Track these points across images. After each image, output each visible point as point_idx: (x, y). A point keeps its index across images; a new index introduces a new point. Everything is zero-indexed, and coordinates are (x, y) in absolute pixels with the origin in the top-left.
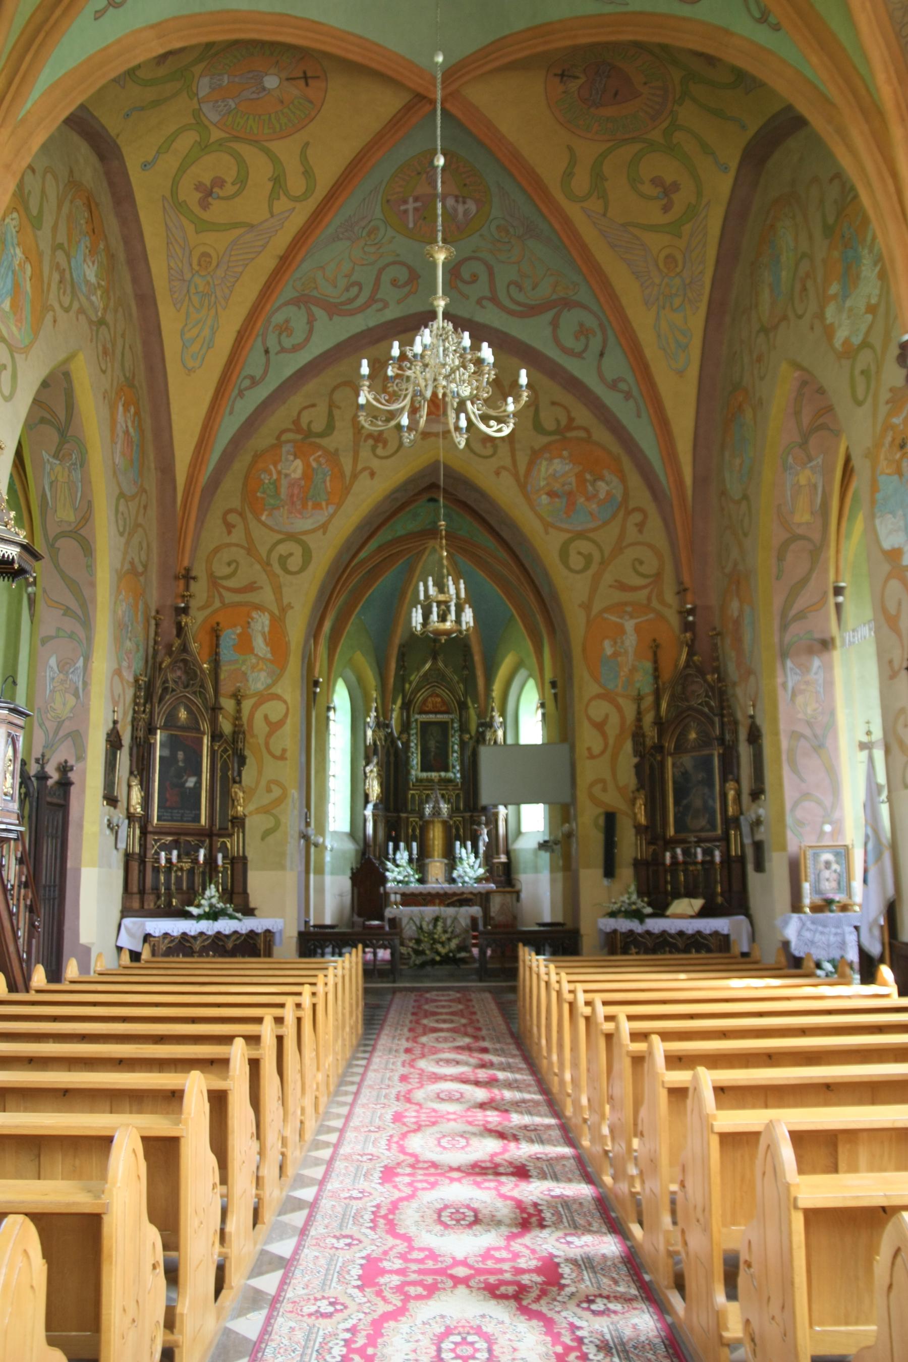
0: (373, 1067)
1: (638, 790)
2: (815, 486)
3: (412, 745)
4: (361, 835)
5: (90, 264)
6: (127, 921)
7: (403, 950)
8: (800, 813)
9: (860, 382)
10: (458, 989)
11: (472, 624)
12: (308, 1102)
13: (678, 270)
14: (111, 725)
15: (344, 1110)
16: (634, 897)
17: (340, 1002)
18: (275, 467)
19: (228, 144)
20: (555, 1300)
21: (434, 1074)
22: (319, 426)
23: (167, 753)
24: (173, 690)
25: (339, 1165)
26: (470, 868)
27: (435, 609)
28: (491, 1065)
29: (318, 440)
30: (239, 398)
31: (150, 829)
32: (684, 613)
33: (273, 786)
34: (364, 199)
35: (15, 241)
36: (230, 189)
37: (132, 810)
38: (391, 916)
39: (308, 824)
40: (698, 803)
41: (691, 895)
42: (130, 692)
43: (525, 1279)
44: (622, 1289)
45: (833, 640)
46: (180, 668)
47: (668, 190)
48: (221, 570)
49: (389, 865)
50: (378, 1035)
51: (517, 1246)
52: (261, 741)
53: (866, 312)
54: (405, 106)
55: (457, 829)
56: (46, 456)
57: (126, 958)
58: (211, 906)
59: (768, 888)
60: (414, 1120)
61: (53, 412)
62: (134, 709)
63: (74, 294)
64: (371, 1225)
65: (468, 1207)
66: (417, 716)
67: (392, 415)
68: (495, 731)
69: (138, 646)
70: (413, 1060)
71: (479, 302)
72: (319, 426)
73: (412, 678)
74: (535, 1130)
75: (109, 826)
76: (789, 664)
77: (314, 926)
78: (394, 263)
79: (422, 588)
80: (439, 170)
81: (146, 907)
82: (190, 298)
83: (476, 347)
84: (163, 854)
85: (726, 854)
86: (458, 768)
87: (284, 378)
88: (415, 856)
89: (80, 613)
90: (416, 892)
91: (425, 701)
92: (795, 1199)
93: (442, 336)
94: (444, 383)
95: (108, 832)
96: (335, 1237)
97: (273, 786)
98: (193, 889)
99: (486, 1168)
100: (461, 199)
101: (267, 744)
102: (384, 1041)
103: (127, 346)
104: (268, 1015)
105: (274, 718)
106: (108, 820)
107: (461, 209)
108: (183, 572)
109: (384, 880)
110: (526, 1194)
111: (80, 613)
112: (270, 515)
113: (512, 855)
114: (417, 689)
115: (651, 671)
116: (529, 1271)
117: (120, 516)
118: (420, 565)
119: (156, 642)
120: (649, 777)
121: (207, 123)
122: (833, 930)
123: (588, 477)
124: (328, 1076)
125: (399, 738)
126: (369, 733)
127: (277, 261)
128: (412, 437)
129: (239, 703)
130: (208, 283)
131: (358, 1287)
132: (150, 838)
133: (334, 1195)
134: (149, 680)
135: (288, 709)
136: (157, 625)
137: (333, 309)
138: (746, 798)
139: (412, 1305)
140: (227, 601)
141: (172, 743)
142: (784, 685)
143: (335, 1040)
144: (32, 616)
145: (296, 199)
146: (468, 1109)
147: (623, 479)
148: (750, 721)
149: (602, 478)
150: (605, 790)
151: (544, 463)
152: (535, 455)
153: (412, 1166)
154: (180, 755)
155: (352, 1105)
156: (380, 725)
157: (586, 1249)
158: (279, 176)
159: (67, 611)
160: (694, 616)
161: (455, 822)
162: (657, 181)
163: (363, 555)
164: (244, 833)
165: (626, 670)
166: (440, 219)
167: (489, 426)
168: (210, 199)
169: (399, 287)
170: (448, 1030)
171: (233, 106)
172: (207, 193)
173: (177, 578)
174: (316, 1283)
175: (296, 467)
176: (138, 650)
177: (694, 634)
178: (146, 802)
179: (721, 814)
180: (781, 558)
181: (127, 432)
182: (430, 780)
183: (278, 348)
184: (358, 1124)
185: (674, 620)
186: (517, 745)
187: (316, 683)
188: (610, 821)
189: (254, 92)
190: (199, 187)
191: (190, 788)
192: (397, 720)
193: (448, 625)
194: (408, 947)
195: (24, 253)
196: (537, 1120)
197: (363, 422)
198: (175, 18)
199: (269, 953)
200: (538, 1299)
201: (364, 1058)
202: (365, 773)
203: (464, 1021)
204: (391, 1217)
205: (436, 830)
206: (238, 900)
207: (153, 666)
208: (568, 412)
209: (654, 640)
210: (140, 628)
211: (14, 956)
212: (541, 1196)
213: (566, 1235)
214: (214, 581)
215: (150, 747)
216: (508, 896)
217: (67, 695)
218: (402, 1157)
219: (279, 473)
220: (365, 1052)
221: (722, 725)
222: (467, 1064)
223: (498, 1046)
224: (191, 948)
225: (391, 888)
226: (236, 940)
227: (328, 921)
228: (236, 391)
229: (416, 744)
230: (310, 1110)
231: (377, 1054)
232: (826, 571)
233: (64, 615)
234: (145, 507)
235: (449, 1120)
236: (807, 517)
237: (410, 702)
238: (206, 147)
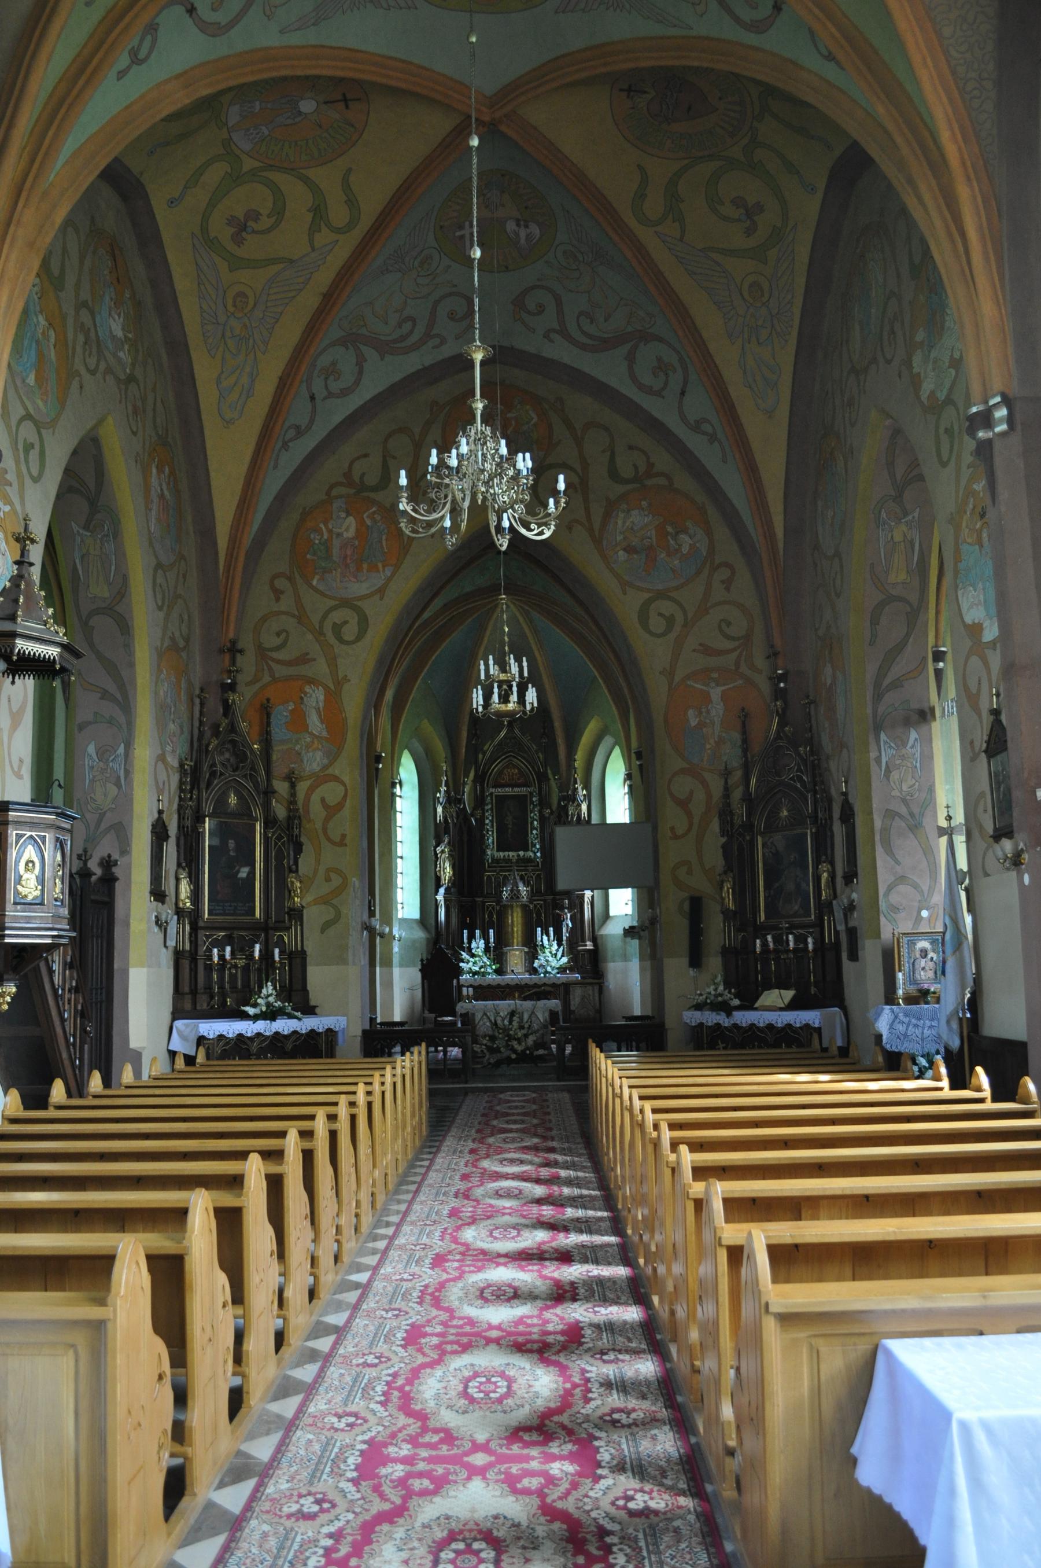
0: (436, 1167)
1: (725, 872)
2: (912, 543)
3: (487, 821)
4: (433, 922)
5: (117, 317)
6: (179, 1024)
7: (477, 1048)
8: (894, 898)
9: (944, 438)
10: (534, 1090)
11: (536, 705)
12: (364, 1196)
13: (765, 300)
14: (156, 815)
15: (403, 1207)
16: (721, 988)
17: (399, 1102)
19: (264, 174)
20: (573, 1353)
21: (496, 1172)
22: (372, 479)
23: (216, 842)
24: (222, 774)
25: (393, 1254)
26: (553, 957)
27: (496, 690)
28: (556, 1164)
29: (372, 495)
31: (201, 924)
32: (776, 679)
33: (333, 875)
35: (38, 308)
36: (265, 222)
37: (181, 905)
38: (463, 1011)
39: (372, 914)
40: (791, 886)
41: (783, 986)
42: (175, 779)
43: (550, 1339)
44: (634, 1345)
45: (932, 710)
46: (228, 750)
48: (270, 641)
49: (465, 955)
50: (444, 1137)
51: (548, 1315)
52: (319, 825)
53: (949, 367)
55: (539, 915)
56: (75, 528)
57: (180, 1063)
58: (268, 1005)
59: (862, 977)
60: (469, 1214)
61: (83, 490)
62: (180, 797)
63: (100, 353)
64: (608, 1540)
65: (510, 1286)
66: (492, 790)
67: (430, 524)
68: (579, 805)
69: (181, 727)
70: (477, 1160)
71: (546, 336)
72: (372, 479)
73: (485, 748)
74: (587, 1221)
75: (157, 923)
76: (883, 736)
77: (381, 1024)
78: (451, 294)
79: (482, 667)
81: (198, 1008)
84: (215, 951)
85: (820, 942)
86: (538, 846)
88: (492, 945)
89: (118, 696)
90: (494, 983)
91: (500, 773)
92: (720, 1238)
94: (483, 489)
95: (156, 929)
96: (384, 1310)
97: (333, 875)
98: (249, 986)
99: (533, 1254)
101: (325, 829)
102: (449, 1142)
103: (159, 400)
104: (321, 1113)
105: (332, 801)
106: (156, 917)
108: (228, 645)
109: (459, 971)
110: (566, 1274)
111: (118, 696)
112: (322, 579)
113: (599, 941)
114: (492, 760)
115: (739, 743)
116: (555, 1333)
117: (158, 589)
118: (492, 622)
119: (201, 723)
120: (738, 860)
121: (238, 152)
122: (928, 1023)
123: (669, 529)
124: (386, 1174)
125: (472, 815)
126: (440, 810)
129: (293, 786)
130: (245, 325)
131: (401, 1346)
132: (201, 934)
133: (387, 1278)
134: (196, 763)
135: (346, 790)
136: (202, 704)
137: (385, 348)
138: (839, 880)
139: (447, 1357)
140: (277, 675)
141: (222, 832)
142: (878, 760)
143: (395, 1139)
144: (67, 700)
145: (339, 231)
146: (525, 1204)
147: (709, 533)
148: (843, 797)
149: (685, 531)
150: (690, 872)
151: (621, 515)
152: (610, 508)
153: (463, 1254)
154: (231, 844)
155: (411, 1203)
156: (452, 800)
157: (610, 1316)
159: (105, 695)
160: (785, 682)
161: (535, 906)
162: (738, 202)
163: (426, 615)
164: (302, 926)
165: (712, 741)
167: (530, 530)
168: (244, 234)
170: (517, 1131)
171: (266, 133)
172: (241, 228)
173: (221, 651)
174: (365, 1343)
176: (182, 732)
177: (785, 702)
178: (196, 895)
179: (814, 898)
180: (875, 621)
181: (162, 496)
182: (507, 860)
184: (414, 1218)
185: (766, 687)
186: (603, 824)
187: (378, 759)
188: (696, 907)
190: (231, 221)
191: (242, 879)
192: (469, 794)
193: (511, 706)
194: (482, 1044)
195: (47, 320)
196: (591, 1213)
198: (202, 65)
199: (331, 1053)
200: (559, 1352)
201: (427, 1159)
202: (436, 854)
203: (535, 1121)
204: (437, 1294)
205: (515, 915)
206: (297, 998)
207: (198, 748)
208: (648, 458)
209: (743, 709)
210: (183, 708)
211: (67, 1063)
212: (579, 1276)
213: (595, 1306)
214: (262, 652)
215: (199, 836)
216: (590, 988)
217: (109, 785)
218: (454, 1246)
219: (330, 531)
220: (430, 1153)
221: (815, 802)
222: (531, 1163)
223: (566, 1145)
224: (248, 1050)
225: (466, 980)
226: (295, 1041)
227: (397, 1018)
228: (280, 444)
229: (492, 821)
230: (366, 1205)
231: (441, 1154)
232: (926, 635)
233: (102, 698)
234: (184, 576)
235: (504, 1214)
236: (902, 576)
237: (484, 773)
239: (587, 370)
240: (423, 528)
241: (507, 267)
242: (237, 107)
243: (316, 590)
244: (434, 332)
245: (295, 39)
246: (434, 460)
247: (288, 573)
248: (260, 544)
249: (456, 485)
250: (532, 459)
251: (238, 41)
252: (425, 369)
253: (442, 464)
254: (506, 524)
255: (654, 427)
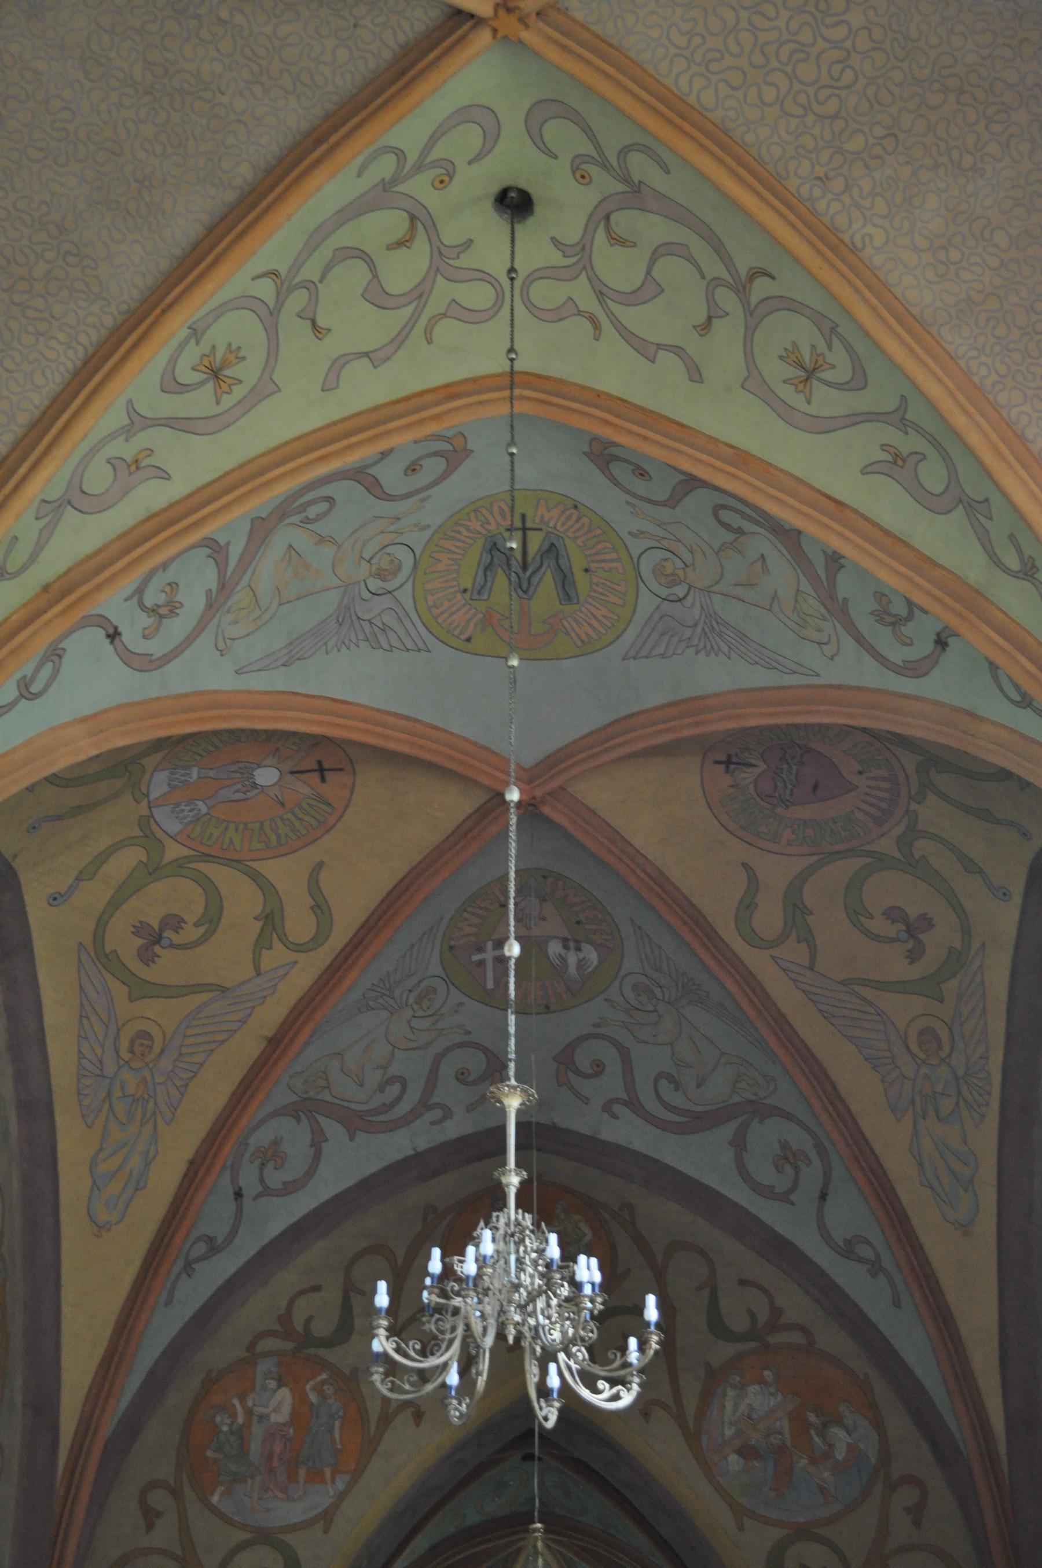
18: (242, 1399)
22: (323, 1328)
29: (322, 1352)
30: (184, 1276)
34: (412, 946)
36: (190, 933)
47: (914, 929)
54: (478, 810)
67: (424, 1376)
71: (607, 1108)
72: (323, 1328)
78: (461, 1045)
80: (513, 962)
82: (110, 1105)
83: (569, 1256)
87: (265, 1241)
93: (514, 1236)
94: (517, 1318)
100: (571, 944)
107: (572, 958)
121: (160, 834)
123: (812, 1418)
127: (265, 1043)
128: (464, 1408)
130: (145, 1079)
137: (356, 1122)
145: (300, 948)
147: (878, 1424)
149: (839, 1422)
151: (731, 1393)
152: (713, 1380)
158: (272, 911)
162: (893, 914)
166: (512, 1042)
167: (596, 1391)
168: (157, 949)
169: (467, 1084)
171: (204, 809)
172: (153, 939)
175: (280, 1403)
183: (260, 1189)
189: (237, 791)
197: (378, 1385)
198: (119, 707)
208: (771, 1300)
219: (249, 1412)
228: (180, 1264)
238: (156, 869)
239: (670, 1160)
240: (412, 1384)
241: (547, 1007)
242: (166, 773)
243: (214, 1510)
244: (435, 1099)
245: (257, 683)
246: (435, 1266)
247: (172, 1482)
248: (131, 1428)
249: (469, 1304)
250: (601, 1268)
251: (176, 680)
252: (418, 1156)
253: (448, 1272)
254: (554, 1381)
255: (779, 1249)
